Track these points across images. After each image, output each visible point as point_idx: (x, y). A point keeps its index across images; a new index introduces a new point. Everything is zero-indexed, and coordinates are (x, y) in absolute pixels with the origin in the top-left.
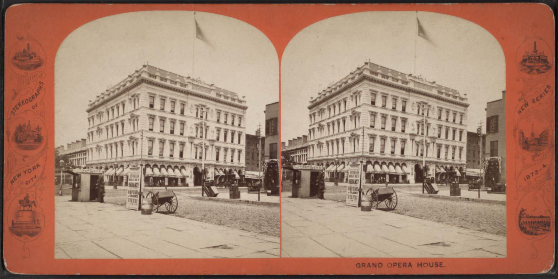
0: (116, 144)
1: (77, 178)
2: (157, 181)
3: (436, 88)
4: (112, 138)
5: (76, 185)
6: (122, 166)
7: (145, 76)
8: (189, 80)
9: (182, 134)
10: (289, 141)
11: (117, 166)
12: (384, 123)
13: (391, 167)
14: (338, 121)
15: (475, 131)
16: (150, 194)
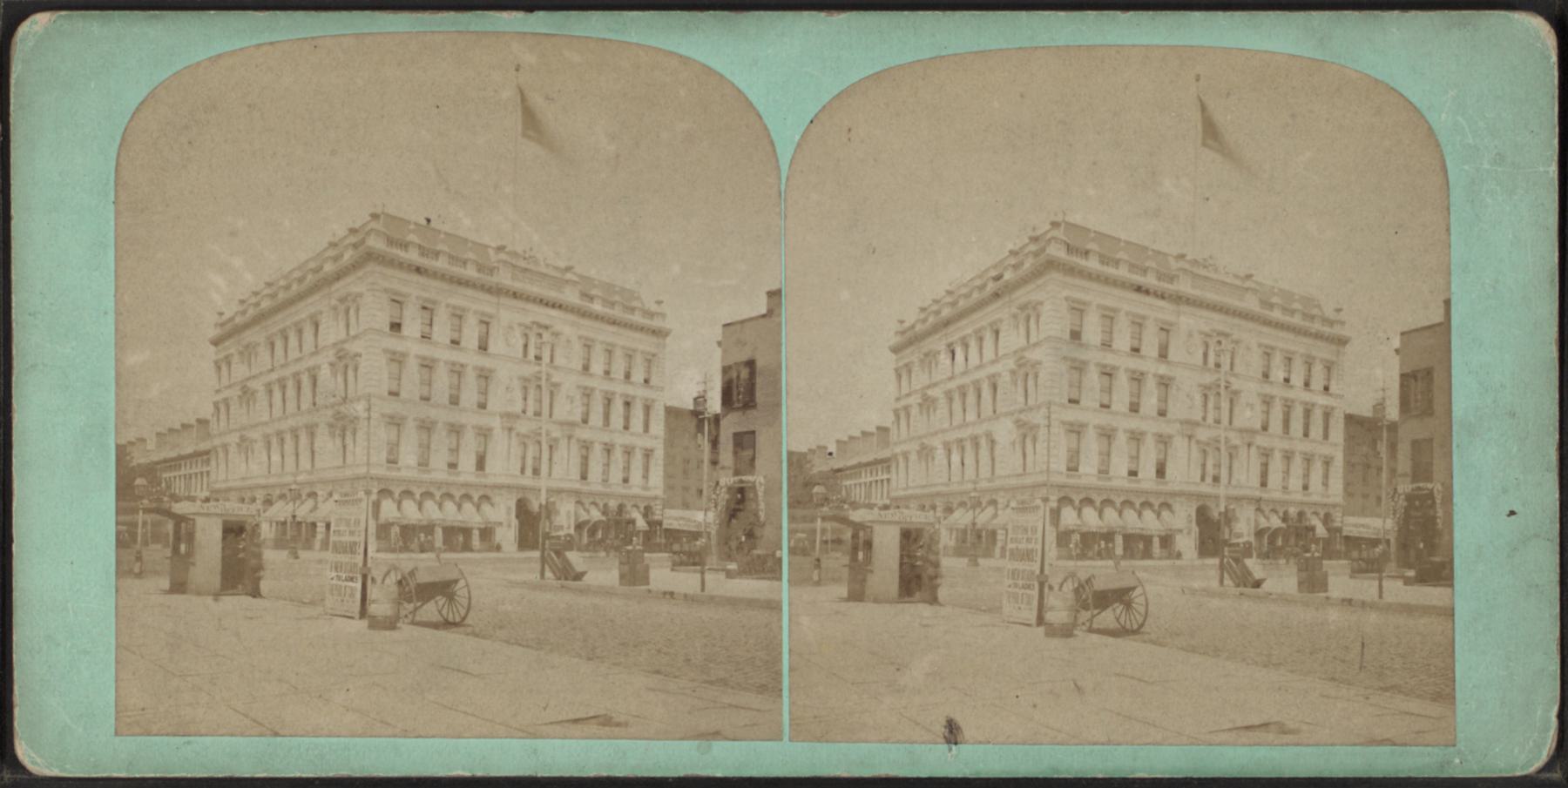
0: (295, 433)
1: (184, 530)
2: (1091, 543)
3: (1255, 291)
4: (964, 425)
5: (183, 548)
6: (313, 495)
7: (1057, 252)
8: (1181, 264)
9: (1162, 413)
11: (980, 503)
12: (1109, 390)
13: (430, 505)
14: (296, 375)
15: (1366, 411)
16: (392, 574)
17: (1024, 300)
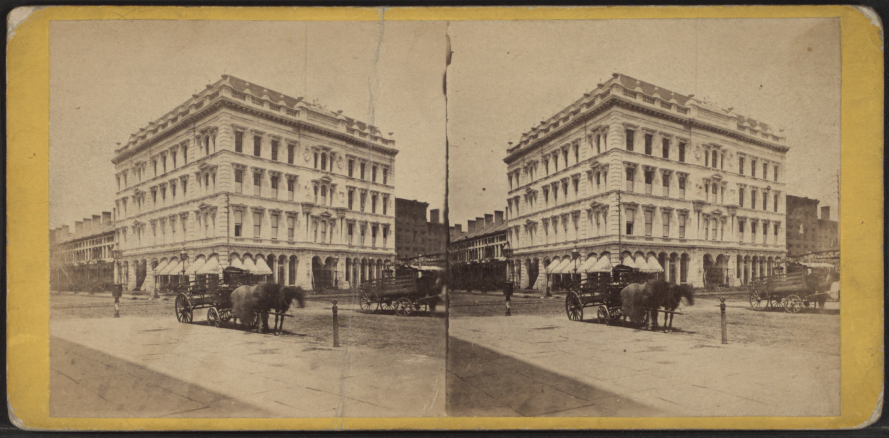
7: (617, 93)
10: (470, 222)
17: (202, 128)
